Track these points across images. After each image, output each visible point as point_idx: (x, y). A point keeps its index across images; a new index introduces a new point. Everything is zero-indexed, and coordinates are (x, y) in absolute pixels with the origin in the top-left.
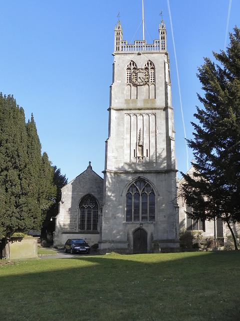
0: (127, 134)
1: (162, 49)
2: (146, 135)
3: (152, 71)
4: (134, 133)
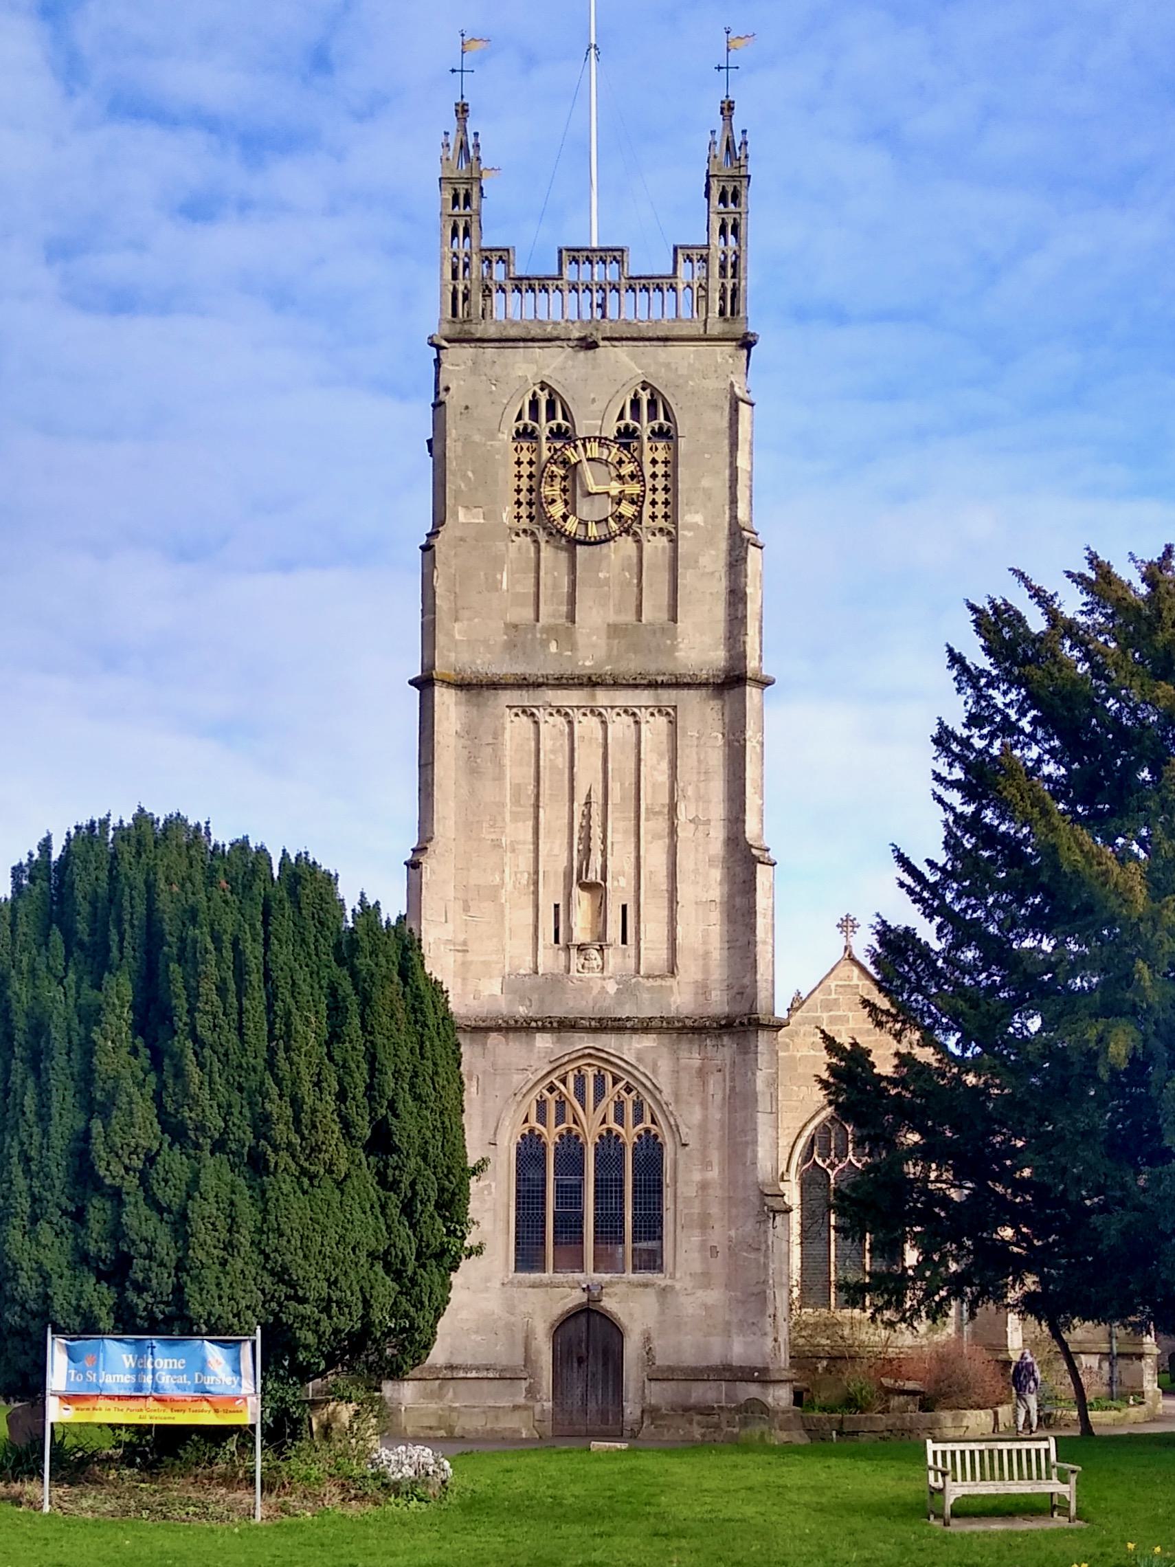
0: (515, 817)
1: (722, 312)
2: (621, 825)
3: (652, 452)
4: (554, 816)
